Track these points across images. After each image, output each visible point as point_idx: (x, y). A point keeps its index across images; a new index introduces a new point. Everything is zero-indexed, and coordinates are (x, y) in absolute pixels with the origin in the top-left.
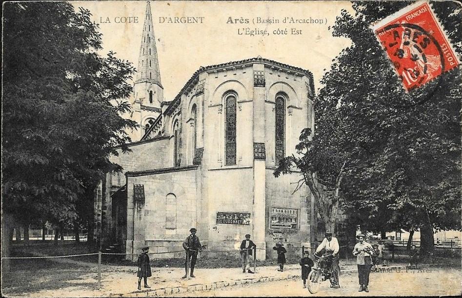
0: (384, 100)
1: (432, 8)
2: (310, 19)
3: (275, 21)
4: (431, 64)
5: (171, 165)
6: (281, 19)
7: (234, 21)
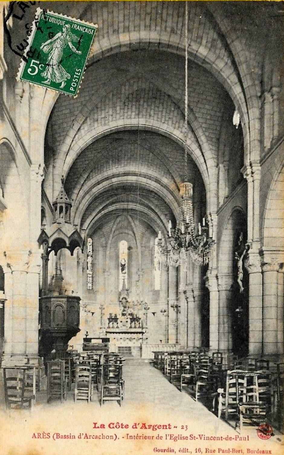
0: (124, 67)
1: (86, 66)
2: (101, 435)
3: (71, 437)
4: (57, 74)
5: (32, 127)
6: (131, 425)
7: (147, 427)
